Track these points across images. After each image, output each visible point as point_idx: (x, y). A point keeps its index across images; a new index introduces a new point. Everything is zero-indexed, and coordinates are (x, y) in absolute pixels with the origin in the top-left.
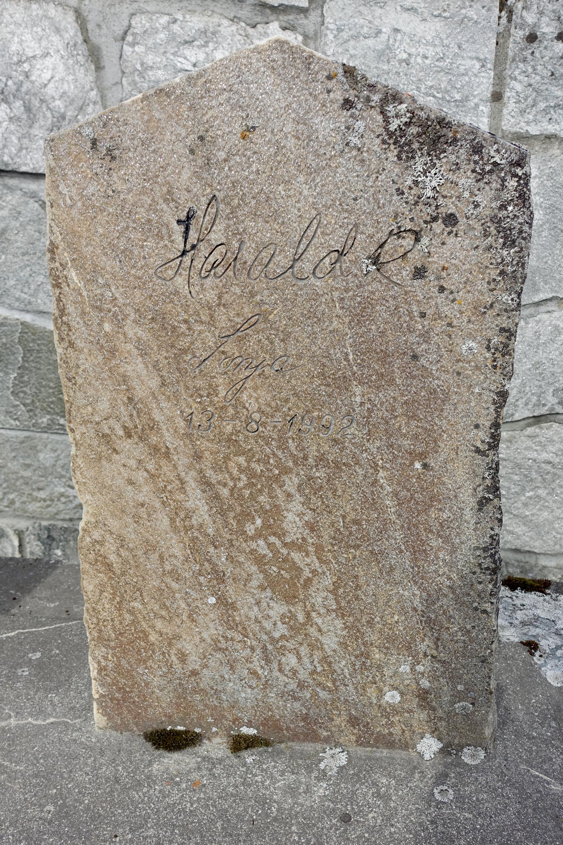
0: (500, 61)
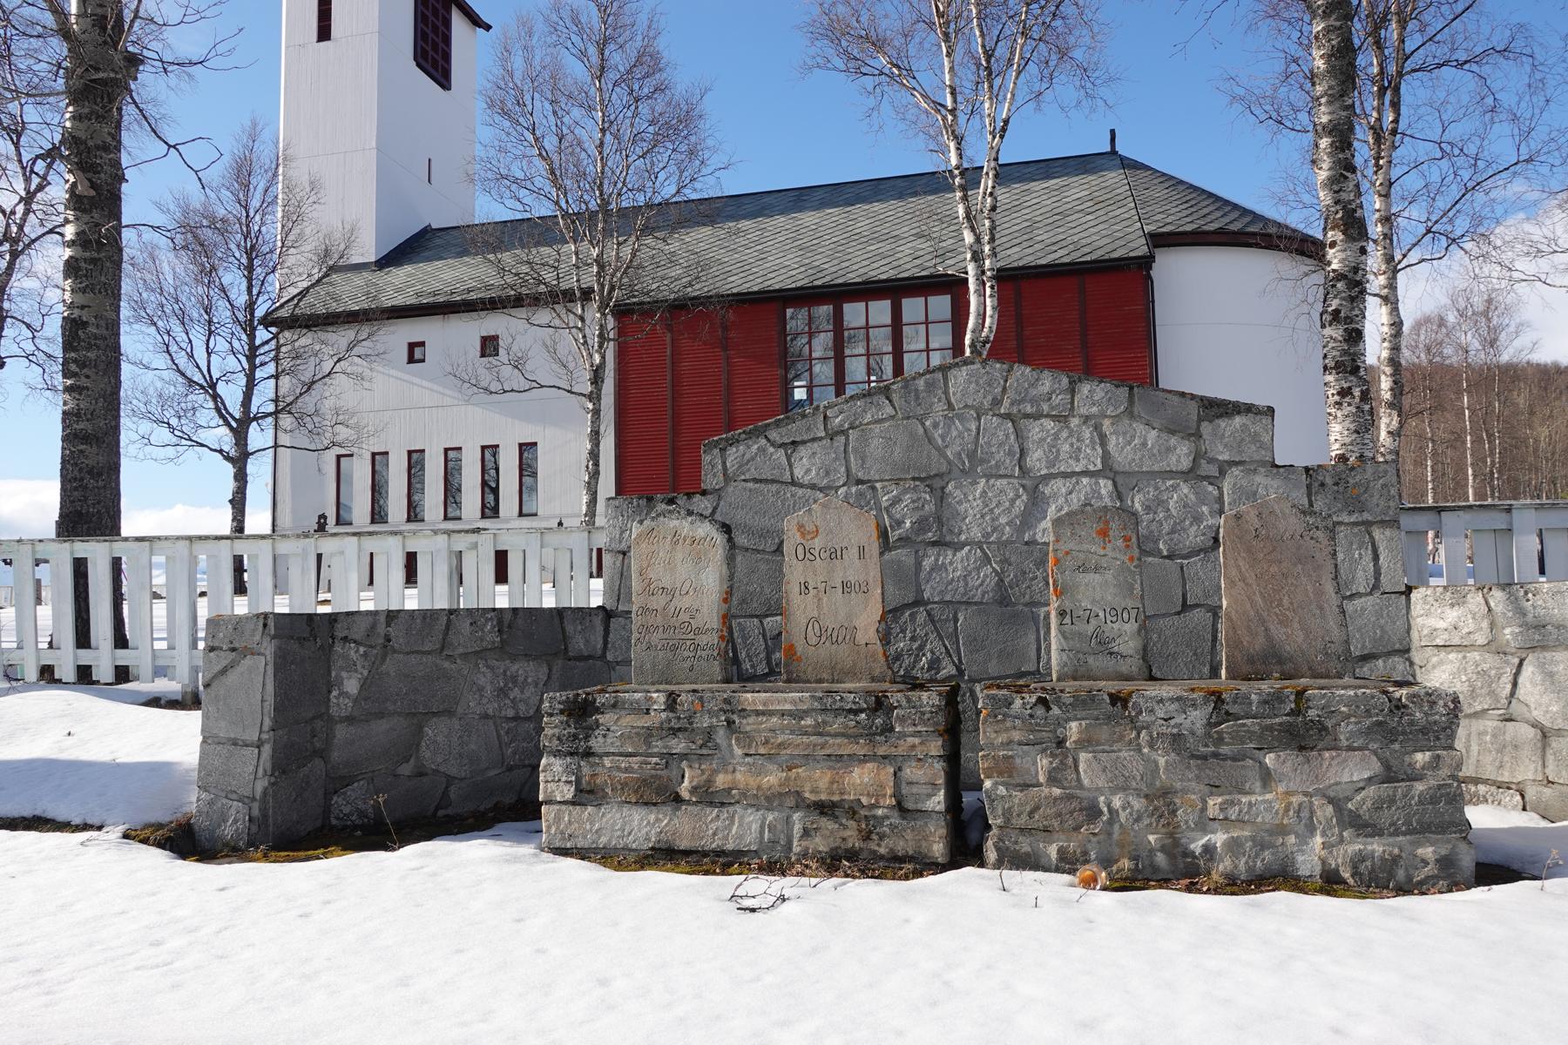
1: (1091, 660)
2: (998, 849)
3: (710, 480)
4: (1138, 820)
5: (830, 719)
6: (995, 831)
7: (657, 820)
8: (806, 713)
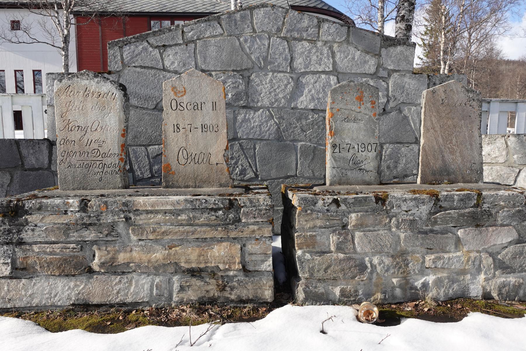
1: (349, 173)
2: (305, 292)
3: (114, 65)
4: (387, 271)
5: (198, 215)
6: (303, 281)
7: (76, 286)
8: (182, 211)
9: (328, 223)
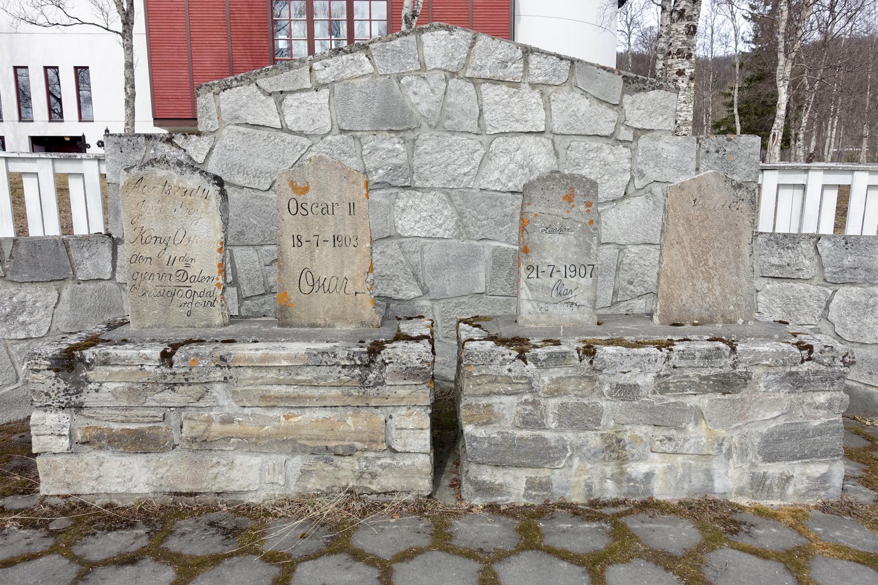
0: (698, 158)
9: (509, 388)
